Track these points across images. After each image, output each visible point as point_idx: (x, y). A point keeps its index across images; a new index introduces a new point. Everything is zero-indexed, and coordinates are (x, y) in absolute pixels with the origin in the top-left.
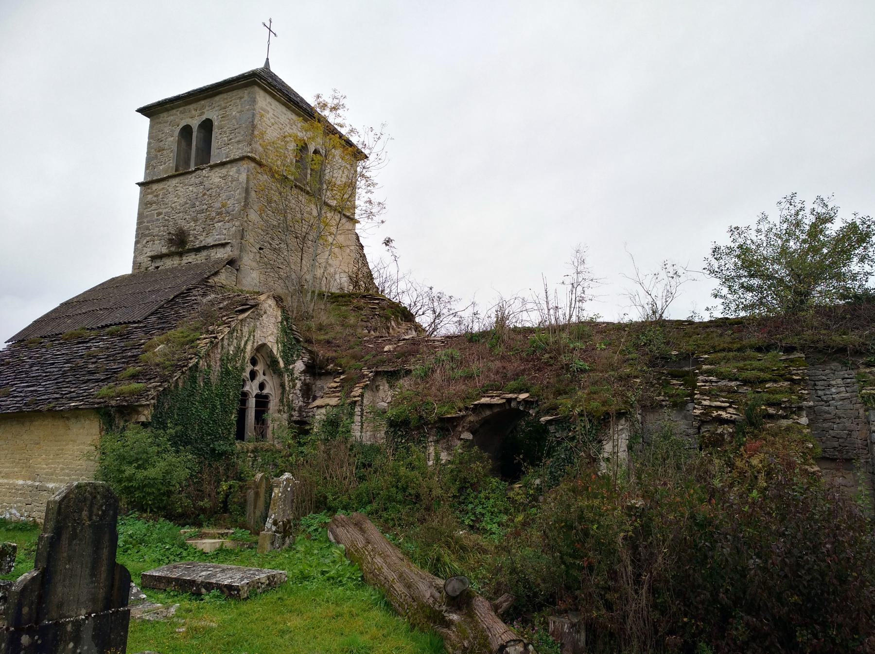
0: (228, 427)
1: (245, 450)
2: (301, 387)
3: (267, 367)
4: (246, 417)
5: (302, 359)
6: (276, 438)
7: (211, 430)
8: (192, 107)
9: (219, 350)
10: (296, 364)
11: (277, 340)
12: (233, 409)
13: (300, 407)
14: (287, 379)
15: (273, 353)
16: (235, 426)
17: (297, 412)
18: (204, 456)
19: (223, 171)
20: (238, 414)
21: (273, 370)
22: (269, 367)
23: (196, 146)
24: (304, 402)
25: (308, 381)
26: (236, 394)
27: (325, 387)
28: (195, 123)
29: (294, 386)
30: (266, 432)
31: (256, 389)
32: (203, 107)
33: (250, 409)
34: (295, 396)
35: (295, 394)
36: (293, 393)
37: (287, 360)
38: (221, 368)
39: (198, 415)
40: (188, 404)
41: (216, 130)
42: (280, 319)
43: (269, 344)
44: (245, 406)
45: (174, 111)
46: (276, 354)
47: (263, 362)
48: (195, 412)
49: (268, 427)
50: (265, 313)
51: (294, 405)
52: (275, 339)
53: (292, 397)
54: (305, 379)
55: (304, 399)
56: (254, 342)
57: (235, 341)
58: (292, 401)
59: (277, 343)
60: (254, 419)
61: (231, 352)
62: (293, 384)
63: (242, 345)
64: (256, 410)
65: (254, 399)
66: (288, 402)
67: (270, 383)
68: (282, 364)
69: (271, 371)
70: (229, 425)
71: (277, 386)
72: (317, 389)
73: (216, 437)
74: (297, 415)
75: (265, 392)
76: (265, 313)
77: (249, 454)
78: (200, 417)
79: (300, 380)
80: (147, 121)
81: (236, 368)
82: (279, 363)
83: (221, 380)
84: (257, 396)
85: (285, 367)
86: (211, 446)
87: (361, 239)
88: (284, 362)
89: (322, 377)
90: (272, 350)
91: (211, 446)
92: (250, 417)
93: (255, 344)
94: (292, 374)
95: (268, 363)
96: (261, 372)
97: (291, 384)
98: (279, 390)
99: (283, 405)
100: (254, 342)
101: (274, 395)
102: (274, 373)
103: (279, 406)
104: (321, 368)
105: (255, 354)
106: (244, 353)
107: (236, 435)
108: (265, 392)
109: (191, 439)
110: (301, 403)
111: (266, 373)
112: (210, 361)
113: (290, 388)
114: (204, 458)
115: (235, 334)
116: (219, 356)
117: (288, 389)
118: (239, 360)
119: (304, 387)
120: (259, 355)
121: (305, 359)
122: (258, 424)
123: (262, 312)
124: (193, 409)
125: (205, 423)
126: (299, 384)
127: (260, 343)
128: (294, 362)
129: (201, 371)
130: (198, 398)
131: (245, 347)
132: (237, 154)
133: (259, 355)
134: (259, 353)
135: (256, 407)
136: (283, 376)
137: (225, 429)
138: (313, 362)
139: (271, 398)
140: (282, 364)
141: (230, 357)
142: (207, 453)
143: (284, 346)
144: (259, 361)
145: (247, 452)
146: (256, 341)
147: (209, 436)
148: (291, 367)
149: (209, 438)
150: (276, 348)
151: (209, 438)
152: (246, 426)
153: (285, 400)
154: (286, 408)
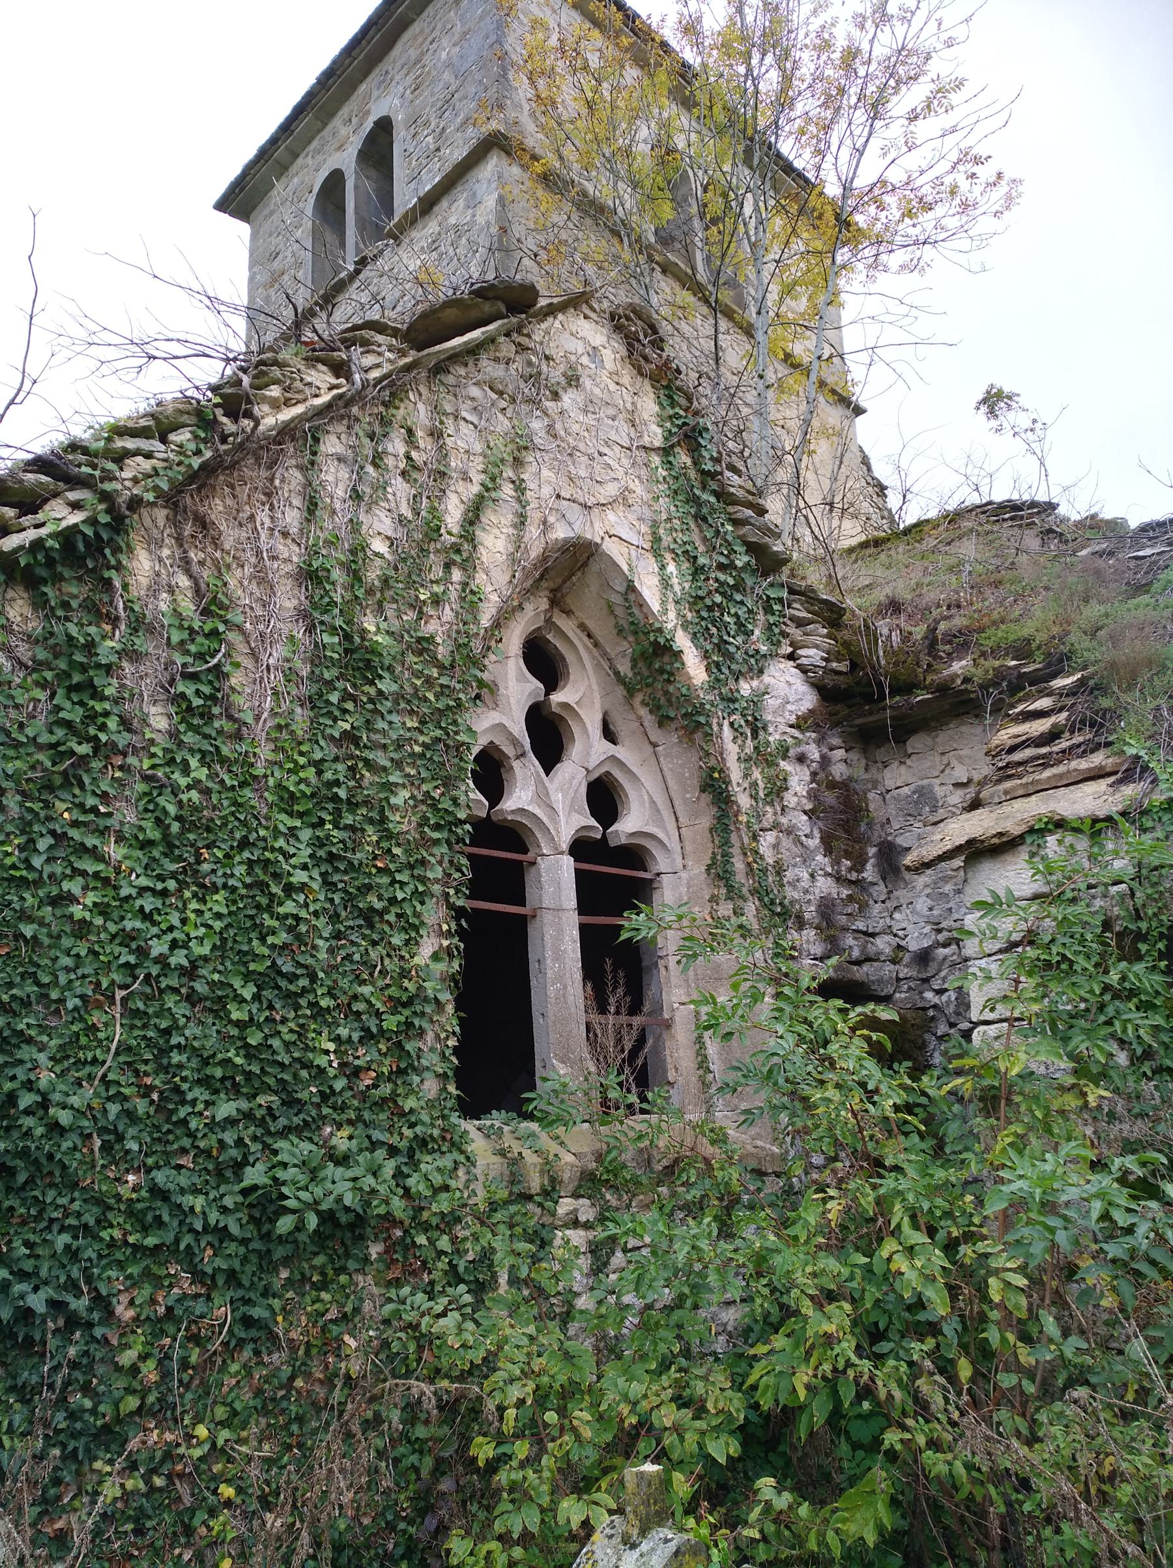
0: (391, 1022)
1: (535, 1183)
2: (812, 795)
3: (620, 691)
4: (533, 966)
5: (791, 657)
6: (724, 1088)
7: (250, 1053)
8: (337, 122)
9: (292, 518)
10: (766, 678)
11: (657, 539)
12: (421, 897)
13: (826, 907)
14: (732, 750)
15: (642, 604)
16: (449, 1019)
17: (810, 934)
18: (189, 1259)
19: (431, 227)
20: (461, 933)
21: (655, 709)
22: (631, 691)
23: (356, 213)
24: (839, 879)
25: (839, 771)
26: (434, 806)
27: (939, 791)
28: (346, 159)
29: (777, 789)
30: (658, 1050)
31: (572, 809)
32: (368, 97)
33: (547, 918)
34: (786, 842)
35: (789, 832)
36: (776, 826)
37: (721, 647)
38: (310, 629)
39: (126, 938)
40: (29, 846)
41: (403, 133)
42: (655, 435)
43: (612, 548)
44: (523, 903)
45: (300, 161)
46: (655, 606)
47: (598, 666)
48: (101, 909)
49: (668, 1025)
50: (573, 380)
51: (791, 893)
52: (644, 529)
53: (776, 846)
54: (825, 761)
55: (836, 862)
56: (521, 521)
57: (400, 489)
58: (779, 870)
59: (656, 552)
60: (578, 976)
61: (379, 546)
62: (769, 779)
63: (453, 514)
64: (583, 928)
65: (568, 864)
66: (755, 870)
67: (649, 781)
68: (695, 668)
69: (643, 712)
70: (397, 1005)
71: (687, 792)
72: (892, 811)
73: (292, 1103)
74: (818, 949)
75: (627, 826)
76: (573, 380)
77: (565, 1206)
78: (143, 953)
79: (801, 759)
80: (240, 230)
81: (424, 646)
82: (678, 654)
83: (312, 702)
84: (581, 848)
85: (715, 684)
86: (255, 1175)
87: (874, 467)
88: (706, 655)
89: (915, 743)
90: (631, 588)
91: (255, 1175)
92: (552, 967)
93: (533, 531)
94: (757, 727)
95: (624, 668)
96: (592, 721)
97: (757, 774)
98: (695, 814)
99: (733, 893)
100: (521, 521)
101: (673, 844)
102: (663, 721)
103: (714, 899)
104: (904, 688)
105: (549, 621)
106: (469, 565)
107: (462, 1076)
108: (627, 826)
109: (55, 1128)
110: (825, 886)
111: (621, 727)
112: (219, 569)
113: (755, 797)
114: (198, 1276)
115: (396, 445)
116: (292, 553)
117: (744, 801)
118: (437, 601)
119: (830, 798)
120: (566, 624)
121: (812, 655)
122: (603, 1009)
123: (556, 374)
124: (74, 886)
125: (192, 999)
126: (799, 781)
127: (561, 532)
128: (756, 666)
129: (138, 624)
130: (127, 815)
131: (468, 535)
132: (457, 153)
133: (566, 624)
134: (568, 613)
135: (582, 909)
136: (708, 735)
137: (368, 1037)
138: (854, 666)
139: (661, 862)
140: (695, 668)
141: (372, 575)
142: (223, 1233)
143: (698, 571)
144: (570, 657)
145: (550, 1192)
146: (534, 516)
147: (236, 1091)
148: (745, 688)
149: (226, 1109)
150: (655, 581)
151: (226, 1109)
152: (537, 1021)
153: (739, 865)
154: (751, 908)
